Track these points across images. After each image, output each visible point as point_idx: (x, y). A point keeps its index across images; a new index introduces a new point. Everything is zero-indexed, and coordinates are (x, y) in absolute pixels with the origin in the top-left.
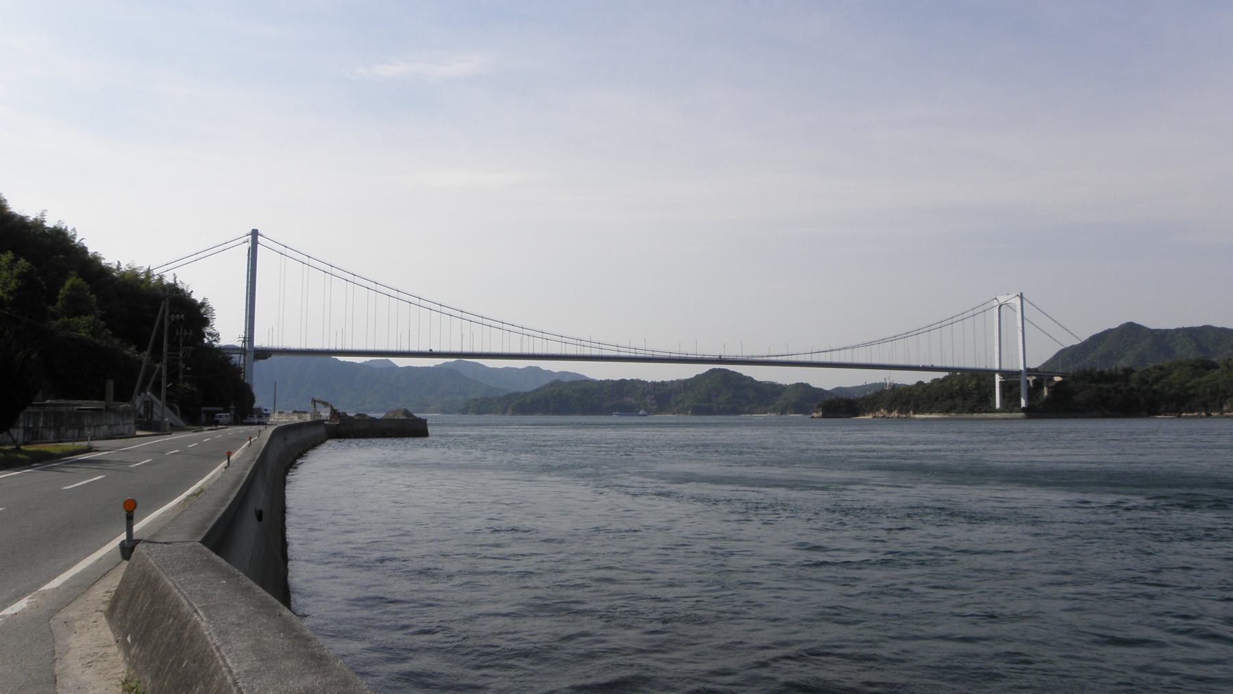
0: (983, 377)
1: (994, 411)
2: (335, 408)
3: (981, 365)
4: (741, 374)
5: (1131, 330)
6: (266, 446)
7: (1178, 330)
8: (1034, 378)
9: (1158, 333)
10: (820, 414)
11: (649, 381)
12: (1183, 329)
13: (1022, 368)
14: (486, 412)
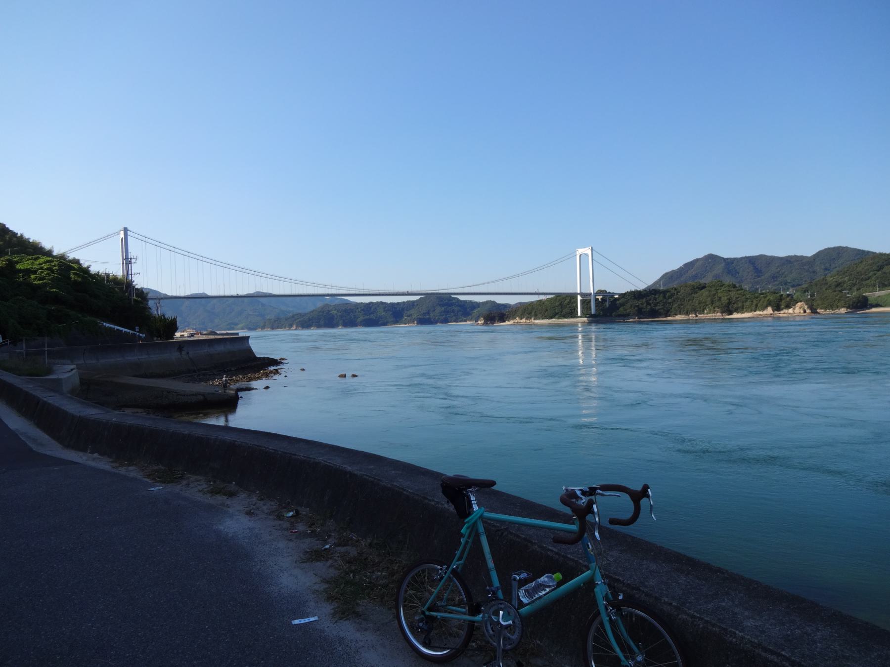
0: (572, 297)
1: (578, 317)
2: (19, 264)
3: (571, 291)
4: (673, 271)
5: (711, 259)
6: (46, 455)
7: (742, 259)
8: (601, 297)
9: (729, 260)
10: (483, 322)
11: (389, 303)
12: (746, 257)
13: (592, 292)
14: (278, 327)
